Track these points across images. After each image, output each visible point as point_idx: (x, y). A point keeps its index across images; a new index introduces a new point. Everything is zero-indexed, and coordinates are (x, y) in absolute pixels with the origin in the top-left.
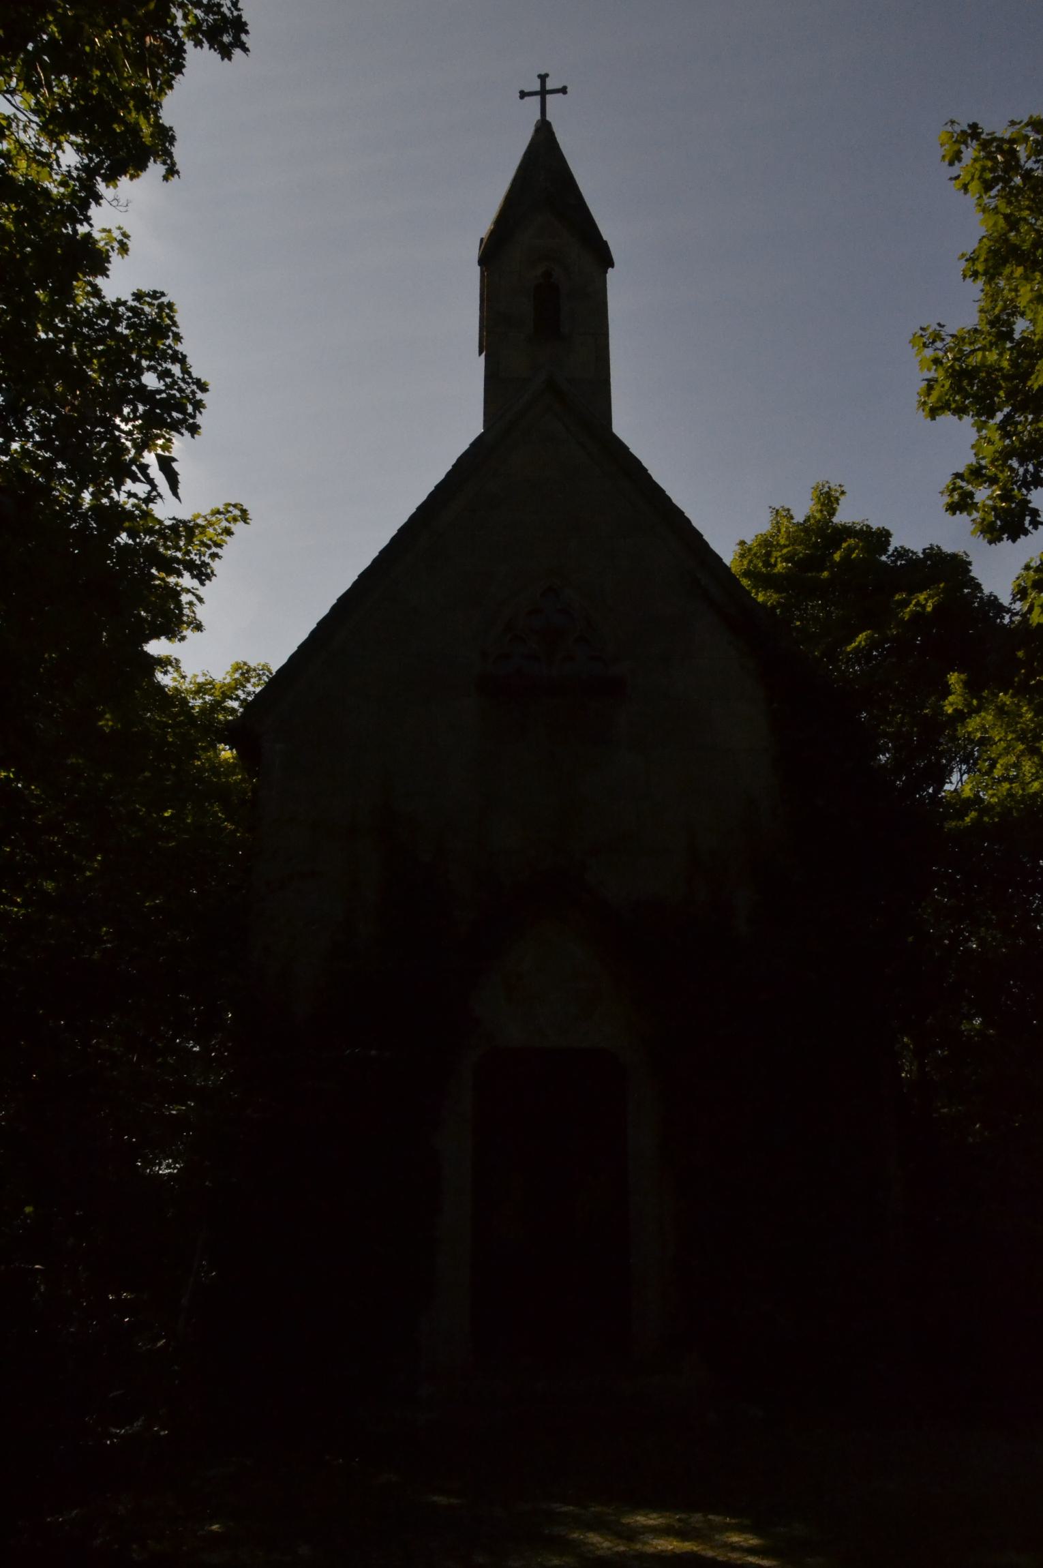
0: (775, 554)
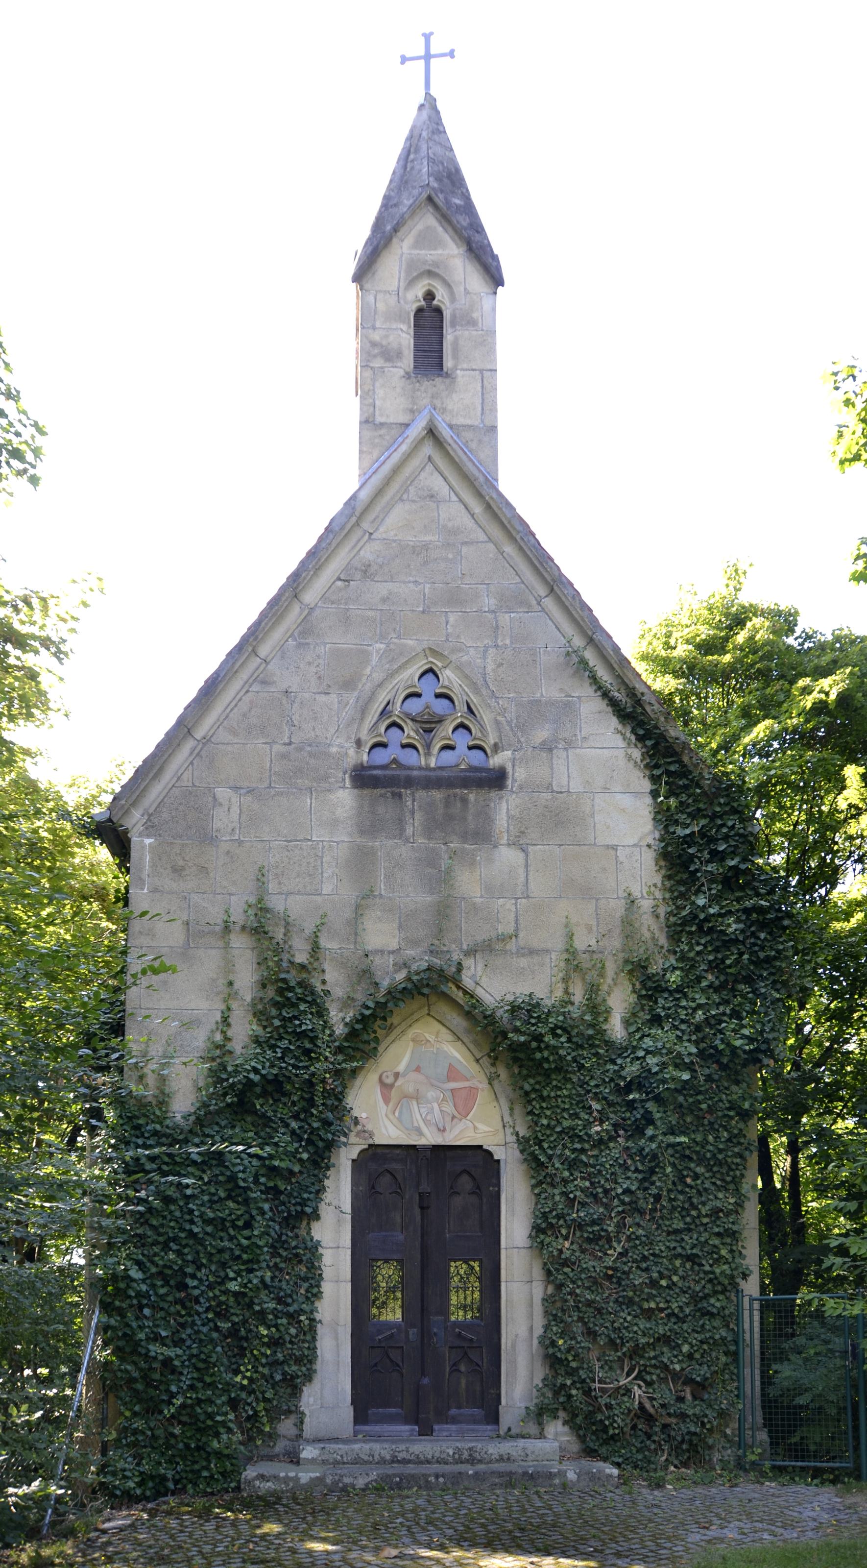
0: (676, 635)
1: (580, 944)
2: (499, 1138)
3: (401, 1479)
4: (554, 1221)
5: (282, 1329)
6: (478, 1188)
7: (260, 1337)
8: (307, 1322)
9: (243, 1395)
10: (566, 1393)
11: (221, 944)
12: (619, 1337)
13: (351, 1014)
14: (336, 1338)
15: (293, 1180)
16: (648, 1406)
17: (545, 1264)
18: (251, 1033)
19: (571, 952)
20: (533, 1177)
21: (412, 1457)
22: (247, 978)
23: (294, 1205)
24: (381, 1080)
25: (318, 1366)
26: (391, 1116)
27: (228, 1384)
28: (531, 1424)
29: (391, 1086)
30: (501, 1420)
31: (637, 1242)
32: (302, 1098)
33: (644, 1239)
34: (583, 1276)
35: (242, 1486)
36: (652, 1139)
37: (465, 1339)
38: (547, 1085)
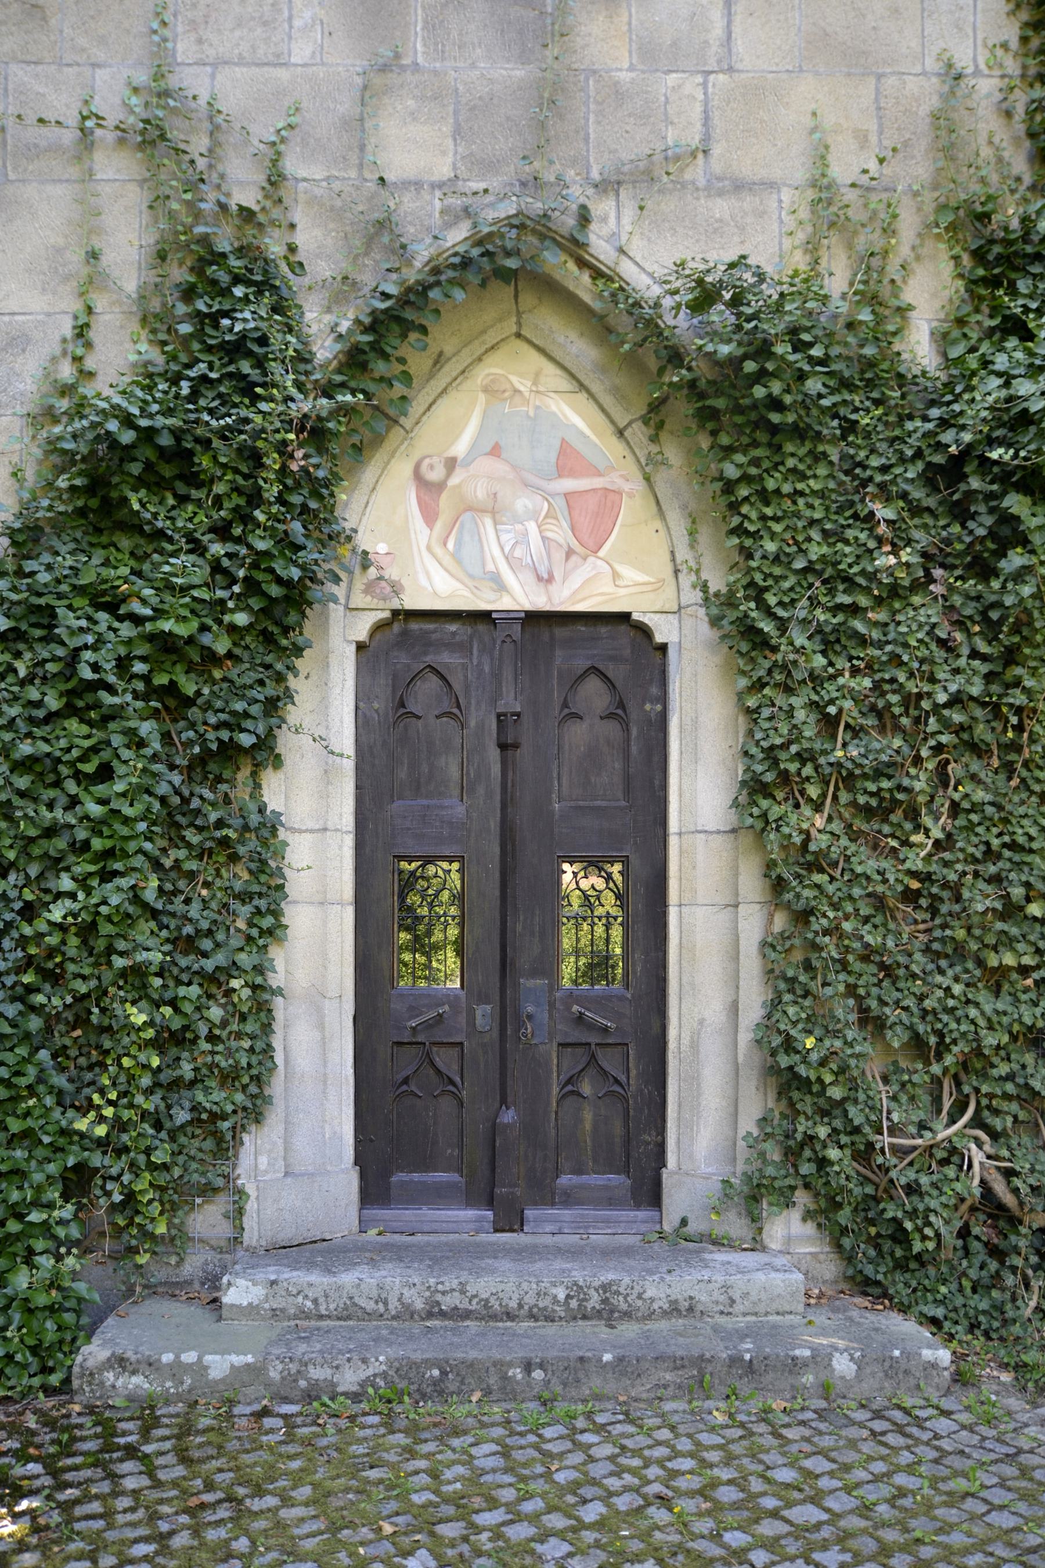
1: (845, 167)
2: (667, 598)
3: (444, 1373)
4: (793, 767)
5: (188, 1008)
6: (621, 705)
7: (130, 1028)
8: (246, 993)
9: (96, 1160)
10: (813, 1146)
11: (74, 172)
12: (935, 1032)
13: (351, 315)
14: (321, 1026)
15: (217, 674)
16: (999, 1187)
17: (770, 865)
18: (133, 358)
19: (823, 191)
20: (743, 673)
21: (474, 1306)
22: (128, 244)
23: (217, 727)
24: (417, 475)
25: (276, 1087)
26: (439, 551)
27: (63, 1132)
28: (732, 1215)
29: (441, 486)
30: (666, 1200)
31: (975, 818)
32: (237, 489)
33: (990, 810)
34: (857, 892)
35: (76, 1383)
36: (1020, 576)
37: (591, 1026)
38: (776, 465)
